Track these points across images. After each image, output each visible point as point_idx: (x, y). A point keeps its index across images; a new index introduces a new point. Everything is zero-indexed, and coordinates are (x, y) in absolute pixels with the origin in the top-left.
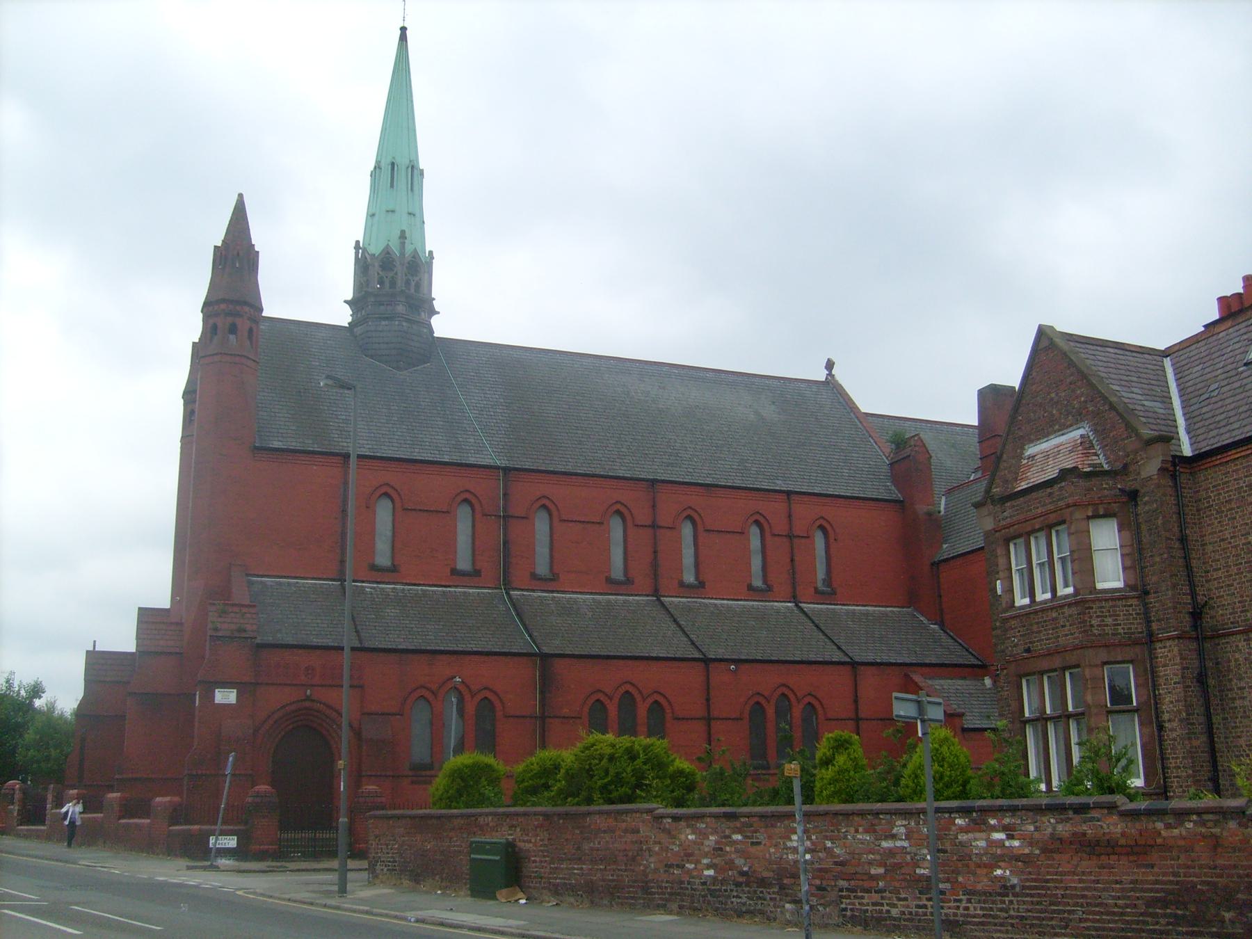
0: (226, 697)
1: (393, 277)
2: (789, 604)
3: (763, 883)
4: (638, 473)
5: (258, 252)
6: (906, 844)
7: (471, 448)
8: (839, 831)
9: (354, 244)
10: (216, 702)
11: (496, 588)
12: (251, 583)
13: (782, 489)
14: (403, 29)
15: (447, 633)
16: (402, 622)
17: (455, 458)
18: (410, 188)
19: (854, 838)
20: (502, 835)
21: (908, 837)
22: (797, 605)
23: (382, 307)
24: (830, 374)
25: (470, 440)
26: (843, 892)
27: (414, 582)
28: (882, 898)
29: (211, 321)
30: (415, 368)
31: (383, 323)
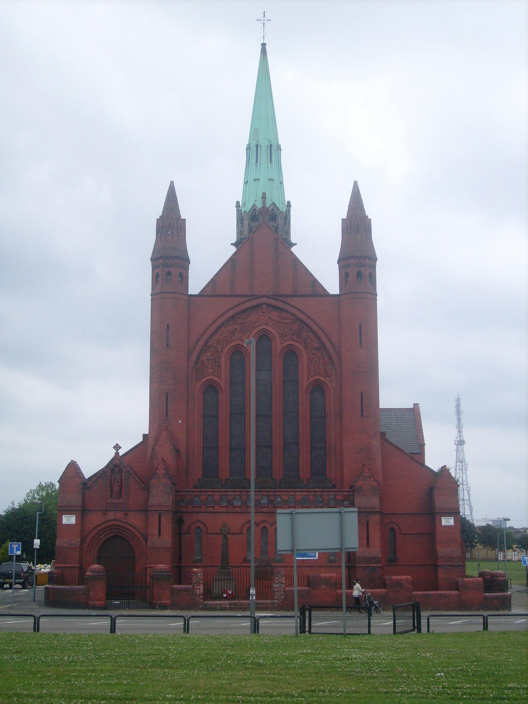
5: (370, 219)
10: (443, 524)
14: (264, 45)
18: (269, 161)
29: (155, 272)
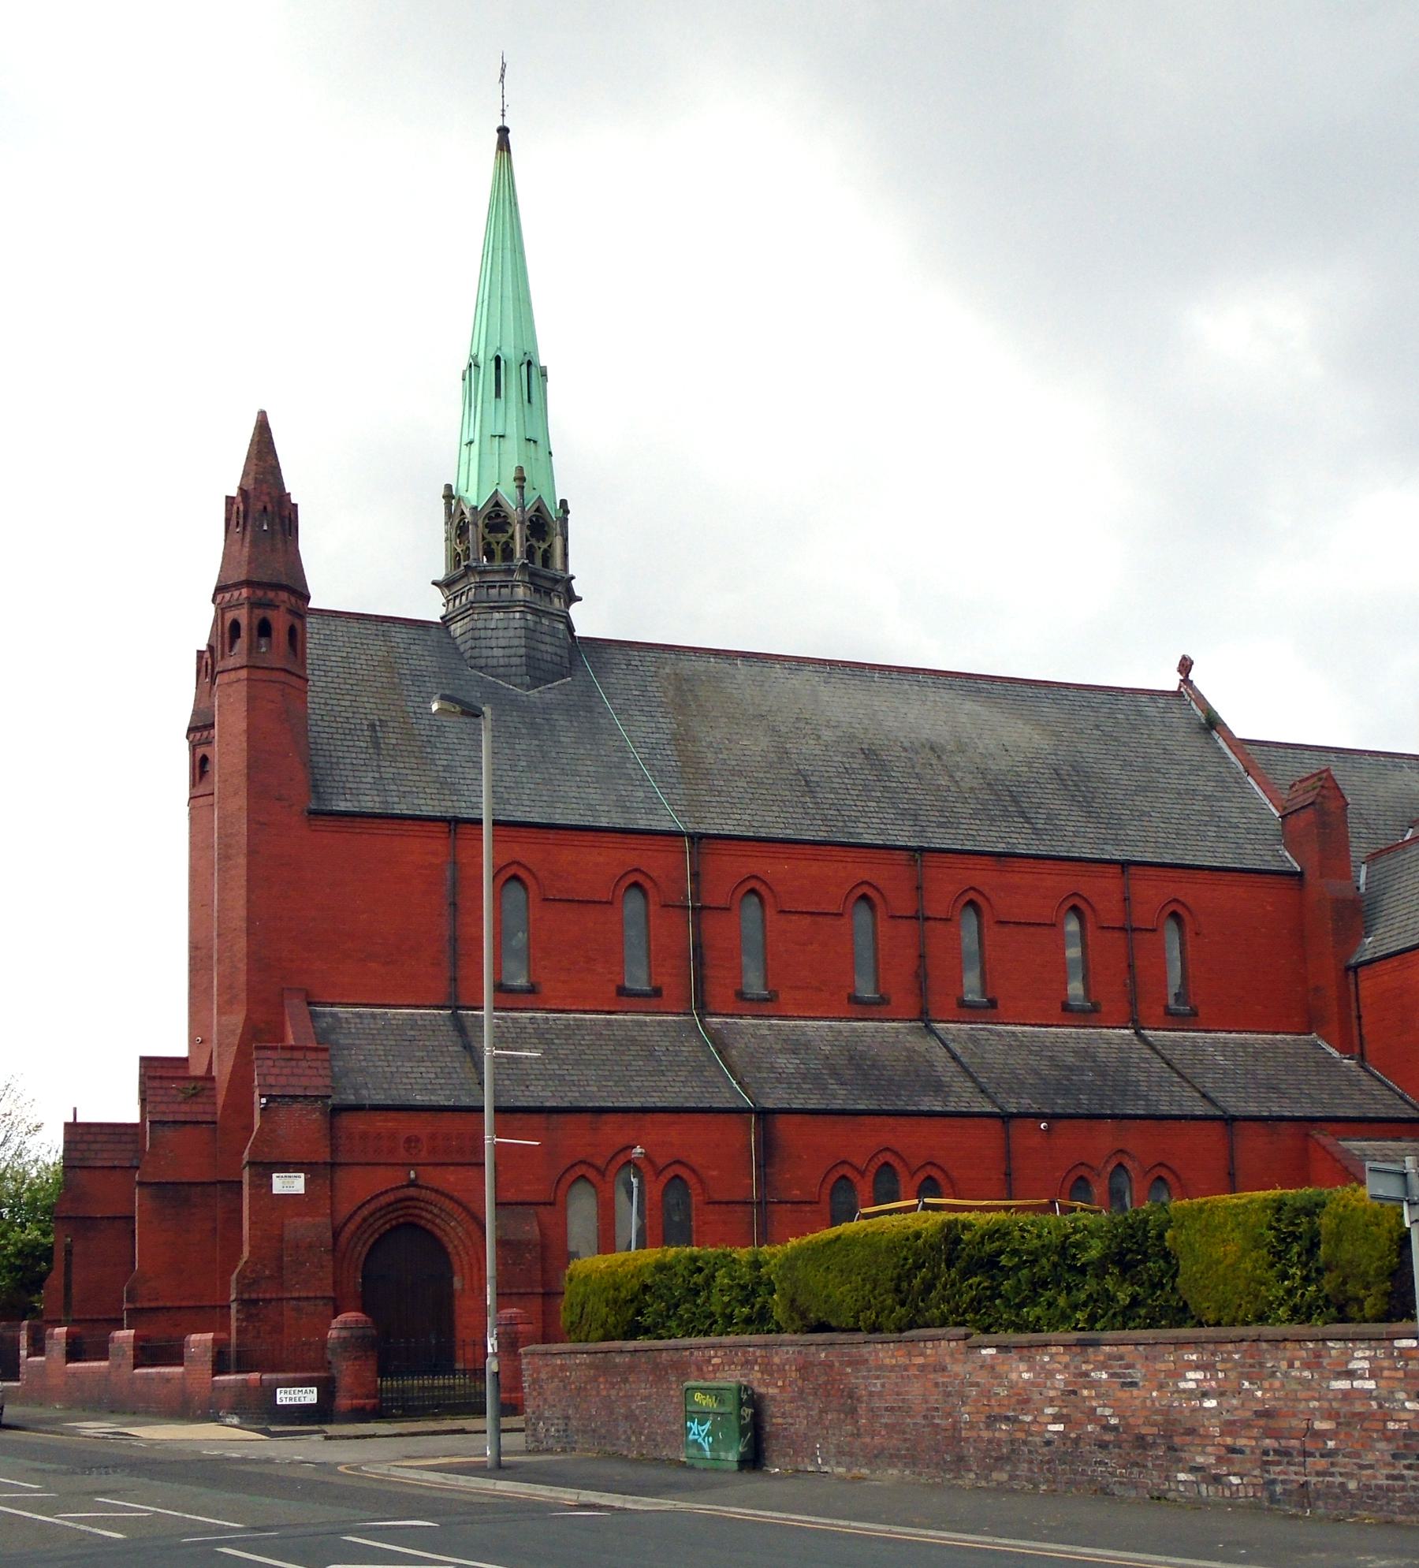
0: (289, 1184)
1: (507, 544)
2: (1127, 1032)
3: (1141, 1442)
4: (894, 838)
6: (1370, 1385)
7: (641, 805)
8: (1262, 1365)
9: (442, 491)
10: (275, 1192)
11: (685, 1014)
12: (314, 1016)
13: (1114, 857)
14: (503, 131)
15: (616, 1082)
16: (548, 1067)
17: (619, 821)
19: (1286, 1375)
20: (731, 1378)
21: (1373, 1375)
22: (1136, 1033)
23: (494, 592)
24: (1186, 681)
25: (638, 794)
26: (1268, 1455)
27: (560, 1007)
28: (1333, 1464)
30: (549, 686)
31: (496, 615)
